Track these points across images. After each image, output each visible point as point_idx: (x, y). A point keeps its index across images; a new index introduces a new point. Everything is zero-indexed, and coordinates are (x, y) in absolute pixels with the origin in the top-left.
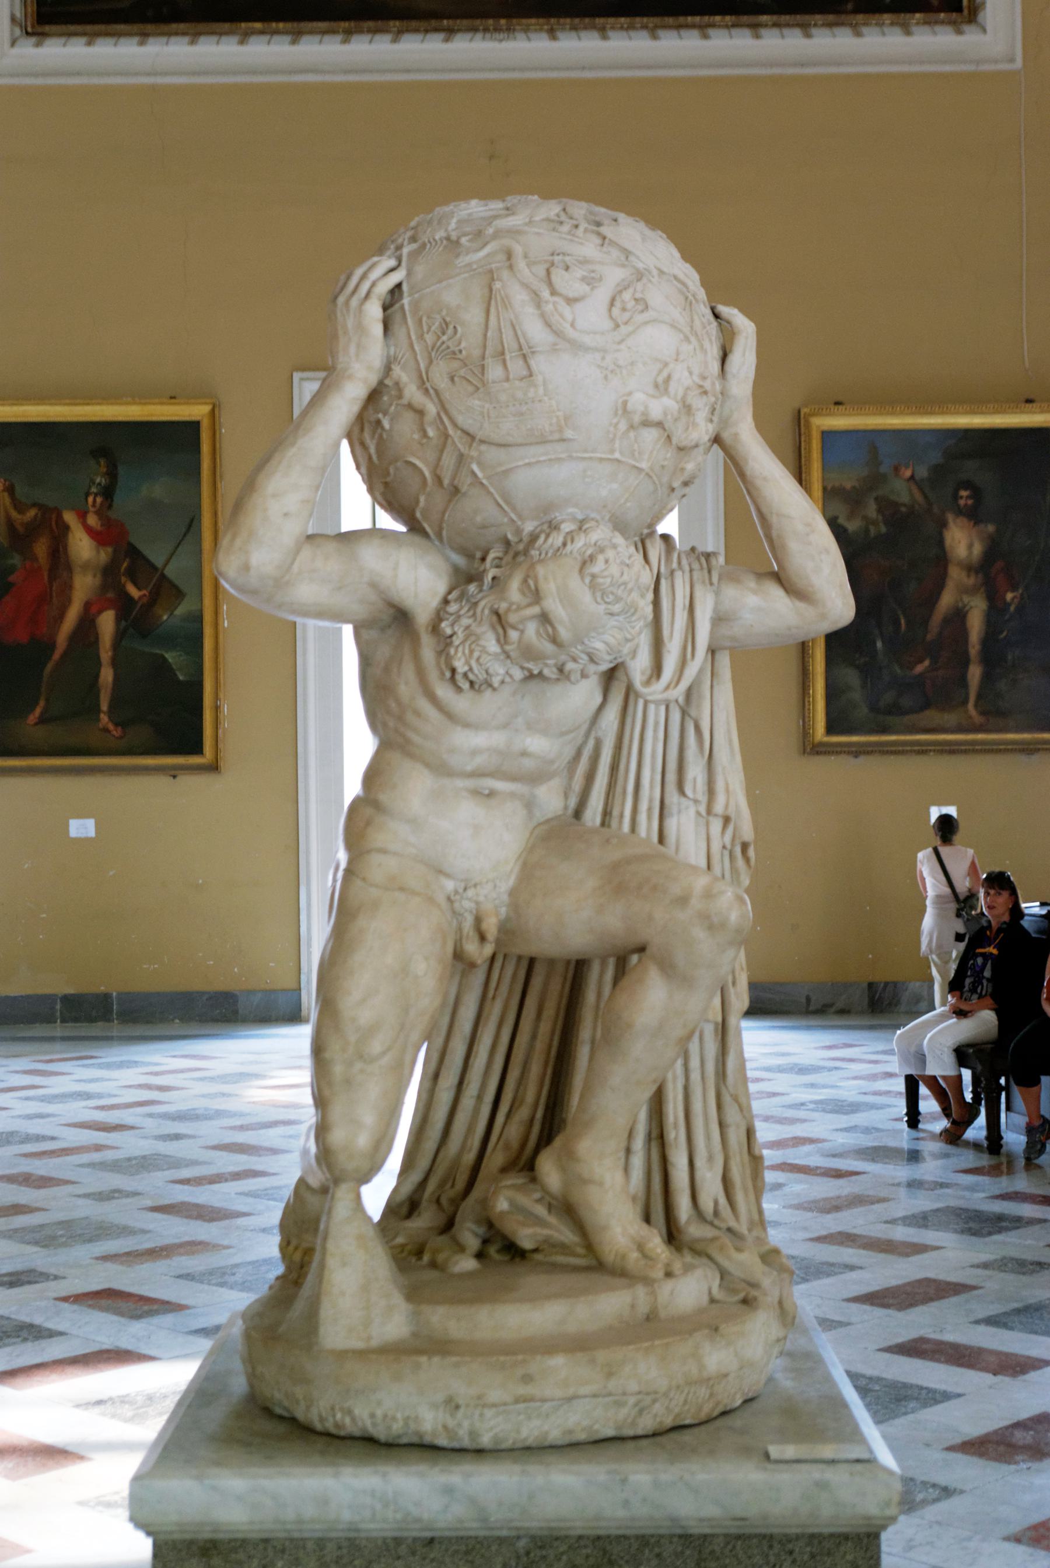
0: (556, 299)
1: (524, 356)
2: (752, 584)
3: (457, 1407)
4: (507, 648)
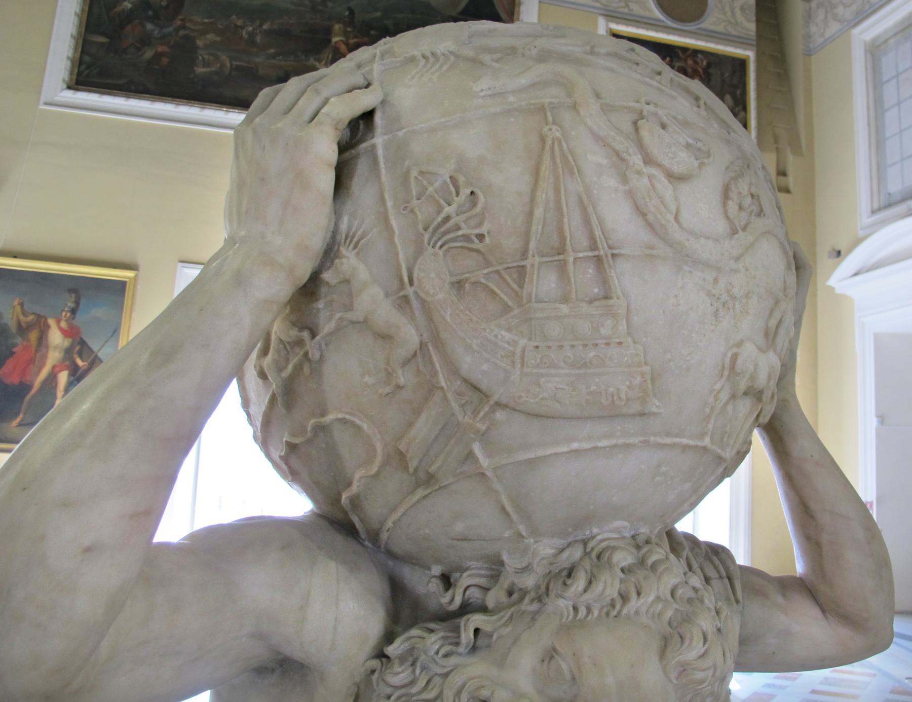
0: (653, 171)
1: (598, 259)
2: (780, 599)
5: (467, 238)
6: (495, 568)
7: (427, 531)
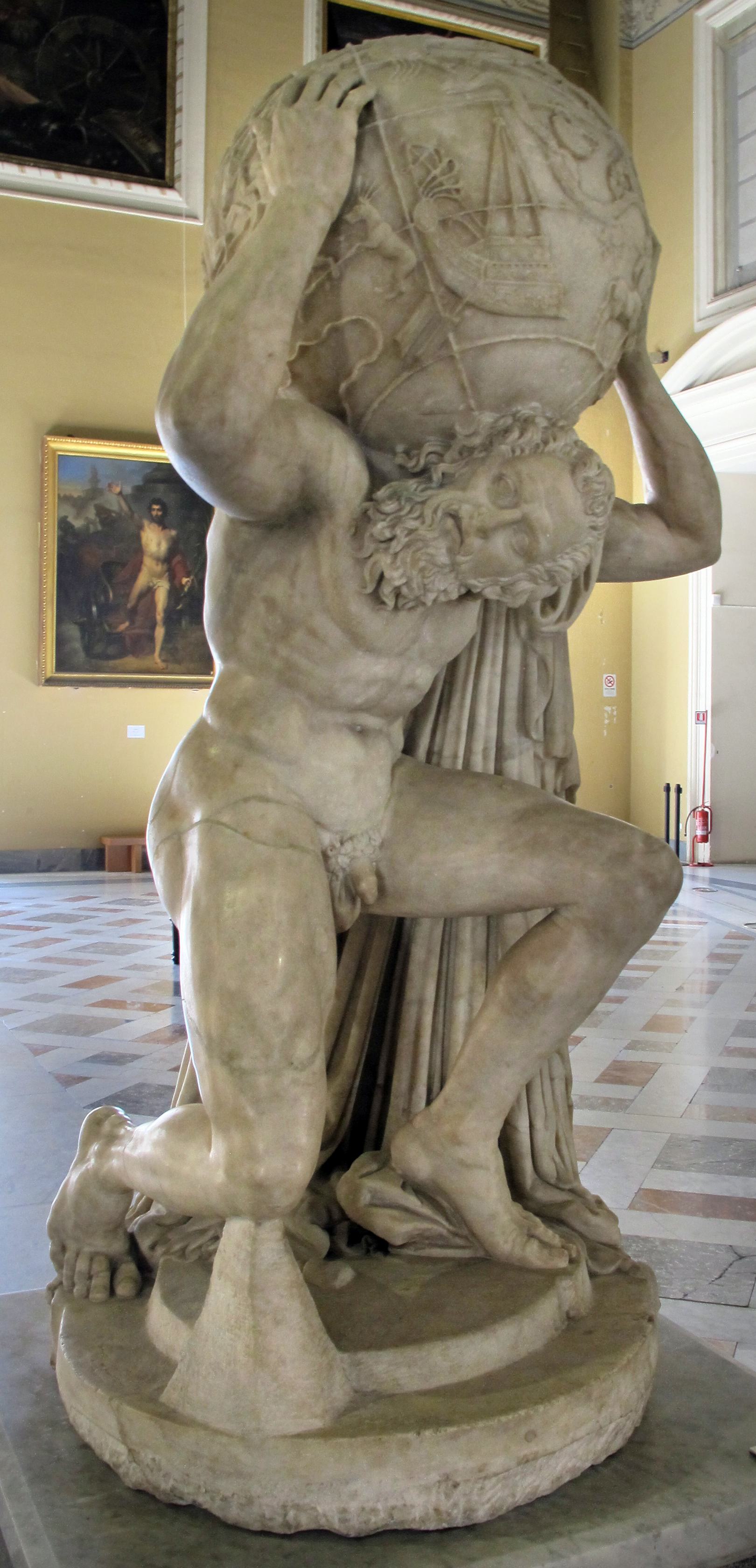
0: (562, 151)
3: (456, 1485)
4: (460, 558)
5: (448, 191)
6: (449, 436)
7: (404, 408)
